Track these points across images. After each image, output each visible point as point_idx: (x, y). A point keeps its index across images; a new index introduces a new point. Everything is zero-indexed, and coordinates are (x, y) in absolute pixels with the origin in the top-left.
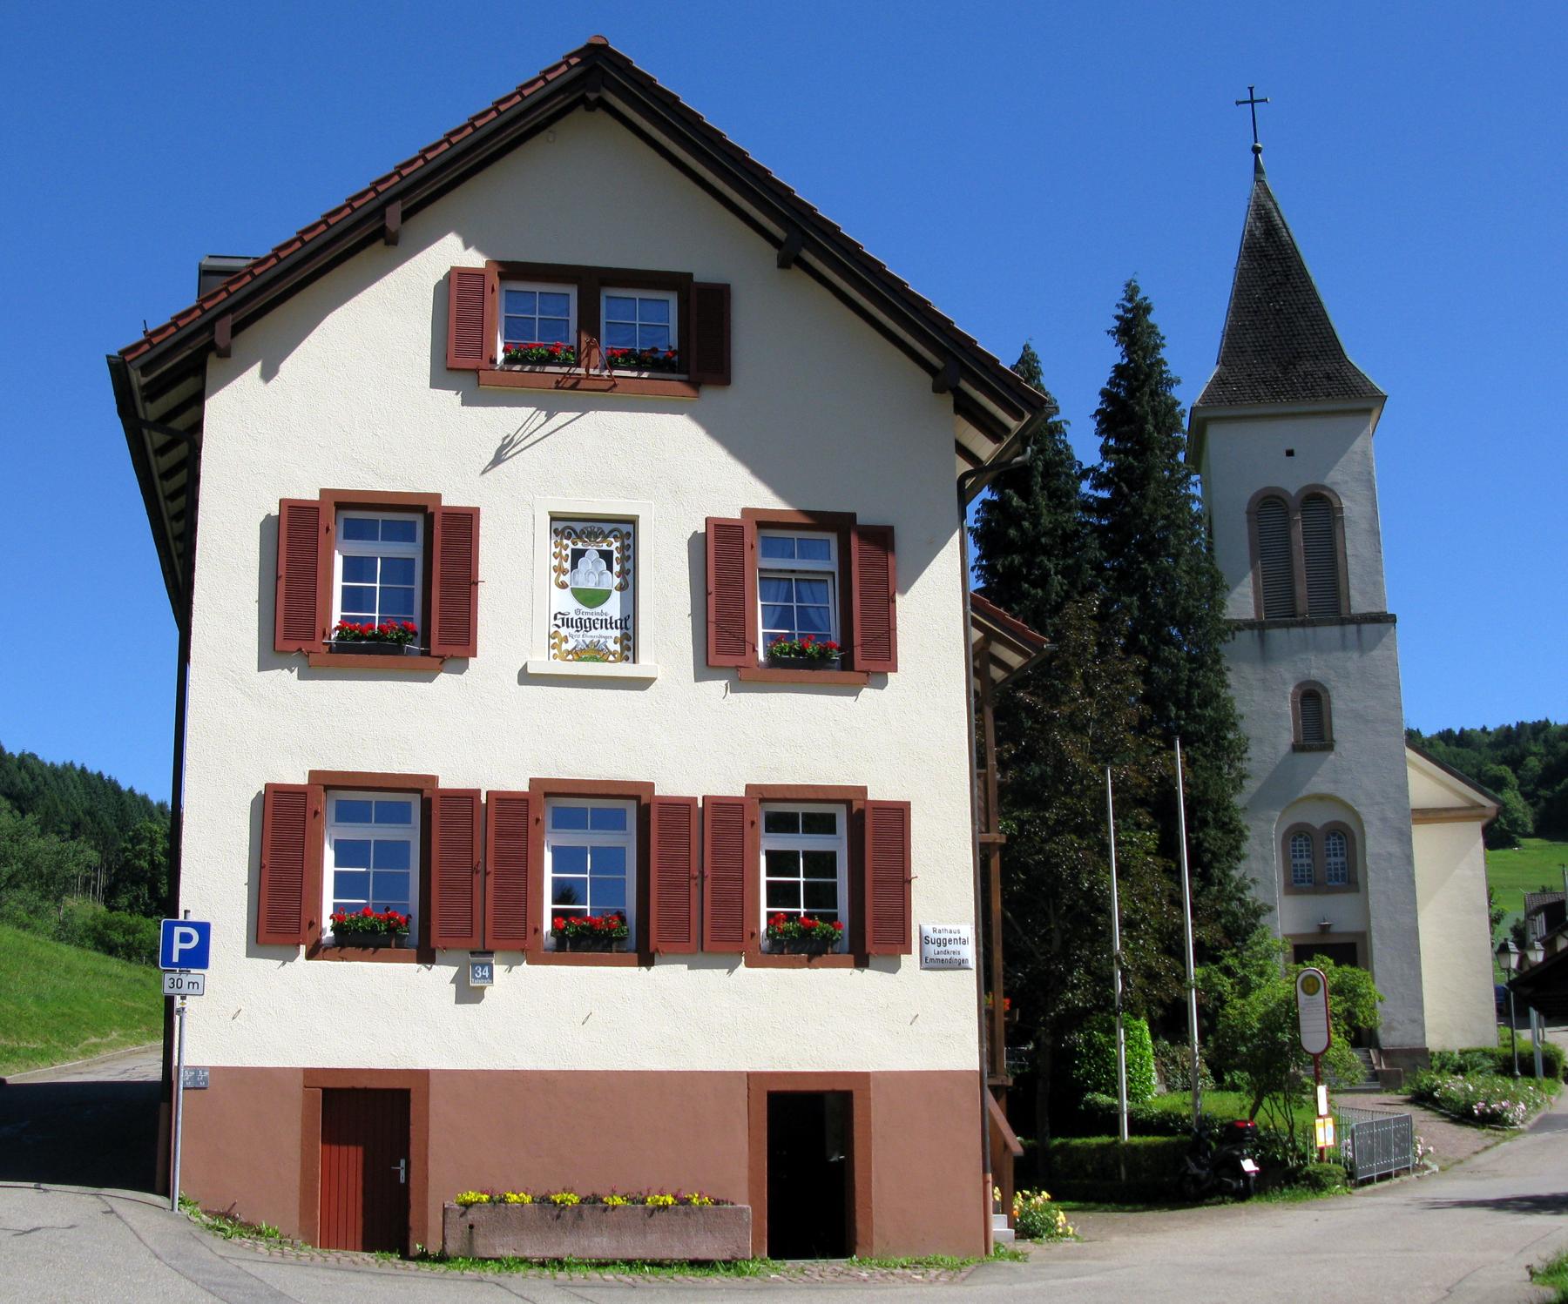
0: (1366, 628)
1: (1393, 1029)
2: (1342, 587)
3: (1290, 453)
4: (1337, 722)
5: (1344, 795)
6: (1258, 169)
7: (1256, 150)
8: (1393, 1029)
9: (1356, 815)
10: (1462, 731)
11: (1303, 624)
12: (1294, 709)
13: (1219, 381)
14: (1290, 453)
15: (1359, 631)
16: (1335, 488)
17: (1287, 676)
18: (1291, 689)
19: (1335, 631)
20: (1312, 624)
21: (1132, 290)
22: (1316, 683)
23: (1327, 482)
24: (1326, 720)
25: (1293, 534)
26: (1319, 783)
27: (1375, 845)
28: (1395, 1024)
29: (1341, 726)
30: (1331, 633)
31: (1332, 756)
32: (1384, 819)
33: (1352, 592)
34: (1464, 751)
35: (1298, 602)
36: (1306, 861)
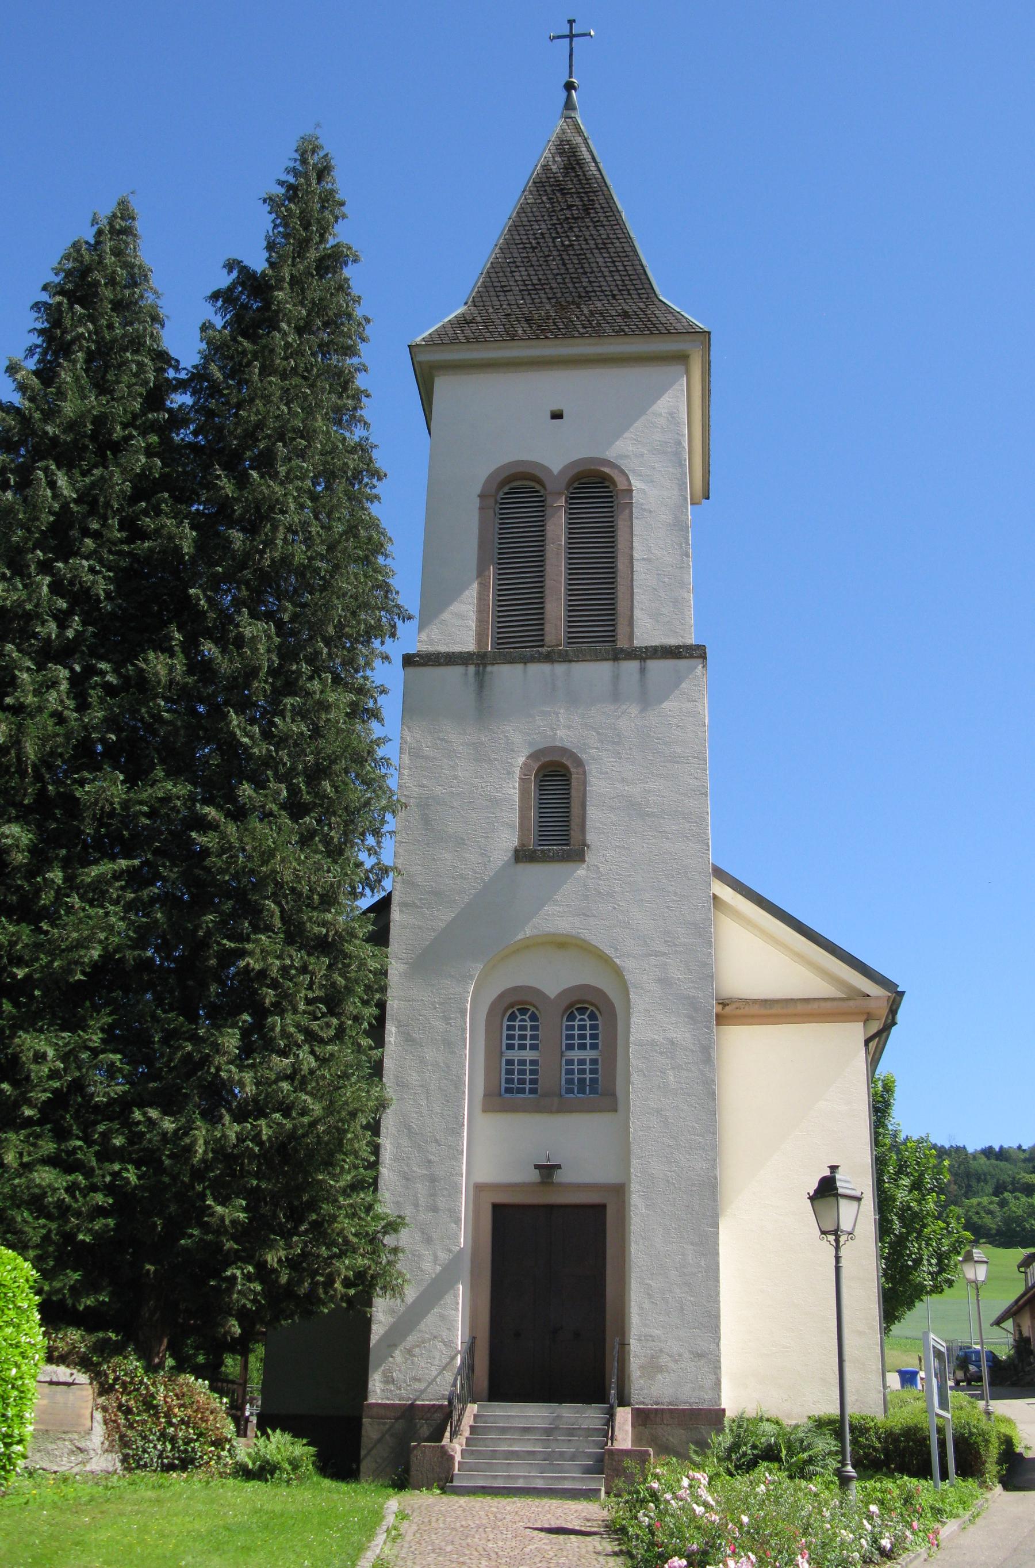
0: (654, 666)
1: (660, 1369)
2: (621, 606)
3: (557, 415)
4: (594, 815)
5: (598, 939)
6: (569, 105)
7: (569, 86)
8: (660, 1369)
9: (618, 972)
10: (1001, 1148)
11: (548, 658)
12: (524, 792)
13: (463, 321)
14: (557, 415)
15: (643, 671)
16: (623, 463)
17: (517, 738)
18: (521, 760)
19: (605, 668)
20: (565, 658)
21: (307, 149)
22: (564, 751)
23: (610, 454)
24: (575, 810)
25: (550, 527)
26: (557, 916)
27: (649, 1026)
28: (664, 1360)
29: (600, 820)
30: (596, 673)
31: (581, 872)
32: (665, 982)
33: (637, 614)
34: (1002, 1164)
35: (548, 628)
36: (528, 1055)
